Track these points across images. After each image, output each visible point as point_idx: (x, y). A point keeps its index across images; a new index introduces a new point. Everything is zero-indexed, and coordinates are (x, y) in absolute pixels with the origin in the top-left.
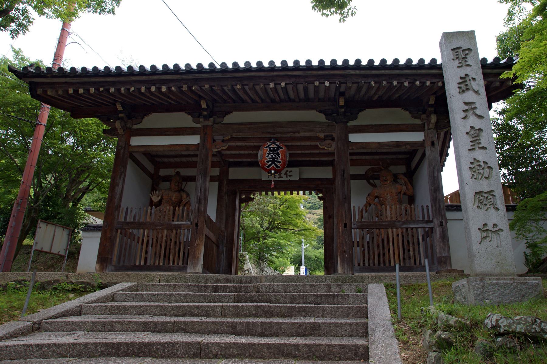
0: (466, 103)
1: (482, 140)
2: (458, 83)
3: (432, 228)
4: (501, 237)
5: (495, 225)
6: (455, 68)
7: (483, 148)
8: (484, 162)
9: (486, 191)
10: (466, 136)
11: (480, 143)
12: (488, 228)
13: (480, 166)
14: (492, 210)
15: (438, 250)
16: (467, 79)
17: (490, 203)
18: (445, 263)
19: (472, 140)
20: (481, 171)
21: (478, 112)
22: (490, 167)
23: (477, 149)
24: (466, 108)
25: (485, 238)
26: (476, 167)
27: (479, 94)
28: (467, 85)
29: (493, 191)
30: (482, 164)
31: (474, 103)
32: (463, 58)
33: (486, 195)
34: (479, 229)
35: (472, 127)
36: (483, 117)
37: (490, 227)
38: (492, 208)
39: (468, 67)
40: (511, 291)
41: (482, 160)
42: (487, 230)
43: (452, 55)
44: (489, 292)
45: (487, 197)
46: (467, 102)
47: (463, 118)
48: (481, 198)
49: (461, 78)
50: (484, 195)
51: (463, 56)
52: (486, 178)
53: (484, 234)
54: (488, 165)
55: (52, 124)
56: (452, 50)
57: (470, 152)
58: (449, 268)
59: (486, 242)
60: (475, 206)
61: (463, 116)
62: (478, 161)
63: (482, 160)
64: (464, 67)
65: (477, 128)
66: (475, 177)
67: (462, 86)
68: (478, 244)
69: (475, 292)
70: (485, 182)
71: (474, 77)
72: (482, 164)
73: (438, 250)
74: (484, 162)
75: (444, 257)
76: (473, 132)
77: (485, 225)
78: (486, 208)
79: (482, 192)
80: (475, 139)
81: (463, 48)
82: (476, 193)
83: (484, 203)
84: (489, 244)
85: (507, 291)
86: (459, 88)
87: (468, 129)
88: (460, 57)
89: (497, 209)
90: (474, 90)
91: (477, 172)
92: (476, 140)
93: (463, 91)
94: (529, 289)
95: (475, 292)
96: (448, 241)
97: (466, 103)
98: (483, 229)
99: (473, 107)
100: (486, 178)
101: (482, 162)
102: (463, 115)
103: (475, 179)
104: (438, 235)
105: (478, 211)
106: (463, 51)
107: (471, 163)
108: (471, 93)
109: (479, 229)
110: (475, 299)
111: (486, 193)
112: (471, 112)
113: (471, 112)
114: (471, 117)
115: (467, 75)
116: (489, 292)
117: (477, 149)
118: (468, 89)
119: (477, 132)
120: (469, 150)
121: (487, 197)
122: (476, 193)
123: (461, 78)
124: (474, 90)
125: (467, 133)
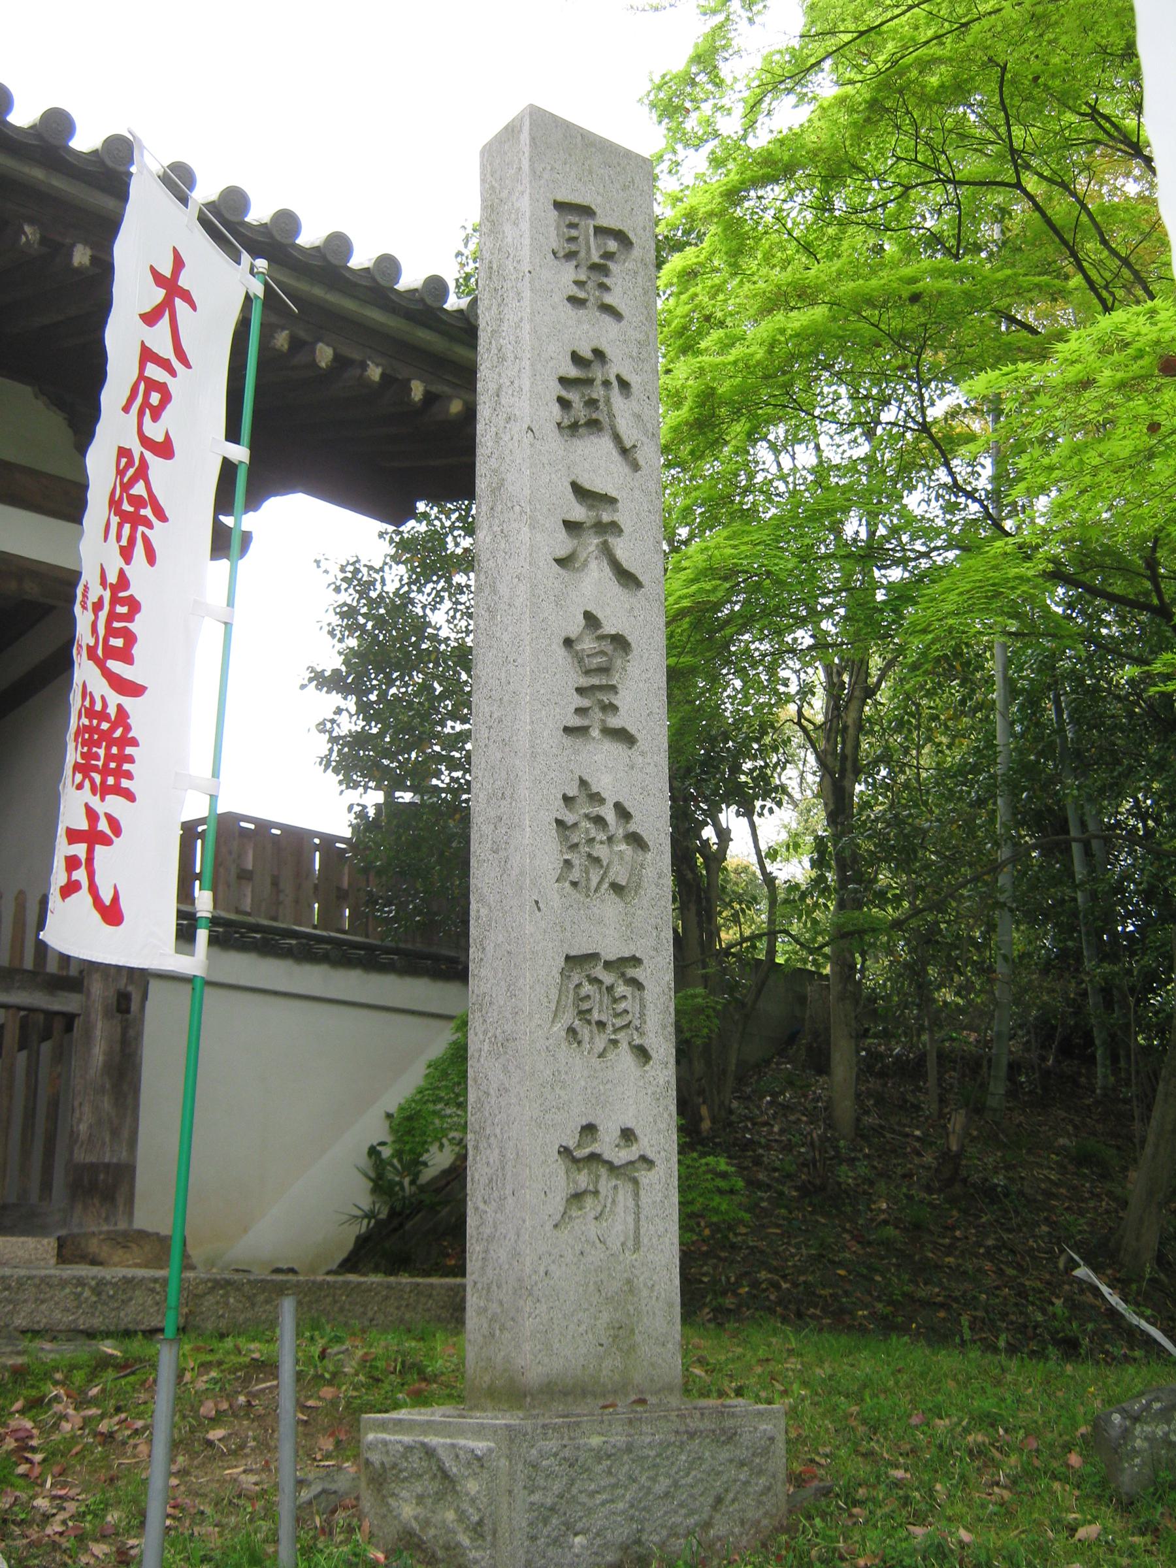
0: (579, 490)
1: (622, 693)
2: (563, 381)
3: (69, 1020)
4: (645, 1199)
5: (628, 1135)
6: (559, 298)
7: (624, 736)
8: (618, 806)
9: (611, 957)
10: (560, 652)
11: (612, 708)
12: (596, 1148)
13: (599, 821)
14: (625, 1058)
15: (83, 1127)
16: (598, 373)
17: (619, 1022)
18: (109, 1197)
19: (585, 682)
20: (601, 851)
21: (622, 549)
22: (635, 840)
23: (595, 733)
24: (578, 512)
25: (577, 1197)
26: (585, 824)
27: (635, 467)
28: (592, 403)
29: (635, 961)
30: (610, 816)
31: (612, 501)
32: (594, 267)
33: (608, 978)
34: (565, 1151)
35: (591, 620)
36: (638, 584)
37: (607, 1145)
38: (624, 1046)
39: (607, 319)
40: (676, 1484)
41: (611, 798)
42: (594, 1157)
43: (553, 232)
44: (592, 1495)
45: (610, 989)
46: (587, 485)
47: (559, 561)
48: (587, 988)
49: (576, 358)
50: (599, 972)
51: (596, 258)
52: (617, 888)
53: (583, 1180)
54: (632, 827)
55: (1040, 1548)
56: (559, 206)
57: (567, 741)
58: (122, 1226)
59: (585, 1223)
60: (559, 1028)
61: (562, 553)
62: (596, 798)
63: (611, 798)
64: (591, 313)
65: (609, 628)
66: (575, 875)
67: (573, 396)
68: (549, 1226)
69: (536, 1497)
70: (610, 908)
71: (626, 377)
72: (610, 816)
73: (83, 1127)
74: (618, 806)
75: (107, 1166)
76: (588, 645)
77: (589, 1129)
78: (600, 1042)
79: (594, 957)
80: (595, 681)
81: (604, 221)
82: (568, 958)
83: (596, 1016)
84: (593, 1229)
85: (663, 1484)
86: (564, 403)
87: (575, 625)
88: (582, 254)
89: (642, 1053)
90: (617, 438)
91: (585, 849)
92: (600, 688)
93: (574, 427)
94: (742, 1464)
95: (536, 1497)
96: (136, 1090)
97: (579, 490)
98: (578, 1154)
99: (606, 518)
100: (617, 888)
101: (610, 804)
102: (563, 544)
103: (574, 884)
104: (98, 1053)
105: (565, 1051)
106: (600, 231)
107: (567, 799)
108: (603, 445)
109: (565, 1151)
110: (533, 1538)
111: (608, 965)
112: (593, 542)
113: (593, 542)
114: (593, 565)
115: (599, 354)
116: (592, 1495)
117: (595, 733)
118: (594, 425)
119: (607, 647)
120: (567, 730)
121: (610, 989)
122: (568, 958)
123: (576, 358)
124: (617, 438)
125: (568, 642)
